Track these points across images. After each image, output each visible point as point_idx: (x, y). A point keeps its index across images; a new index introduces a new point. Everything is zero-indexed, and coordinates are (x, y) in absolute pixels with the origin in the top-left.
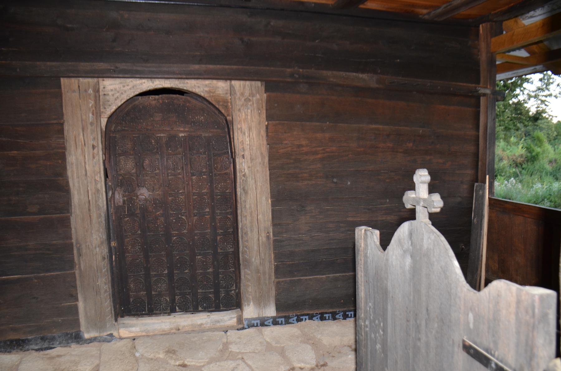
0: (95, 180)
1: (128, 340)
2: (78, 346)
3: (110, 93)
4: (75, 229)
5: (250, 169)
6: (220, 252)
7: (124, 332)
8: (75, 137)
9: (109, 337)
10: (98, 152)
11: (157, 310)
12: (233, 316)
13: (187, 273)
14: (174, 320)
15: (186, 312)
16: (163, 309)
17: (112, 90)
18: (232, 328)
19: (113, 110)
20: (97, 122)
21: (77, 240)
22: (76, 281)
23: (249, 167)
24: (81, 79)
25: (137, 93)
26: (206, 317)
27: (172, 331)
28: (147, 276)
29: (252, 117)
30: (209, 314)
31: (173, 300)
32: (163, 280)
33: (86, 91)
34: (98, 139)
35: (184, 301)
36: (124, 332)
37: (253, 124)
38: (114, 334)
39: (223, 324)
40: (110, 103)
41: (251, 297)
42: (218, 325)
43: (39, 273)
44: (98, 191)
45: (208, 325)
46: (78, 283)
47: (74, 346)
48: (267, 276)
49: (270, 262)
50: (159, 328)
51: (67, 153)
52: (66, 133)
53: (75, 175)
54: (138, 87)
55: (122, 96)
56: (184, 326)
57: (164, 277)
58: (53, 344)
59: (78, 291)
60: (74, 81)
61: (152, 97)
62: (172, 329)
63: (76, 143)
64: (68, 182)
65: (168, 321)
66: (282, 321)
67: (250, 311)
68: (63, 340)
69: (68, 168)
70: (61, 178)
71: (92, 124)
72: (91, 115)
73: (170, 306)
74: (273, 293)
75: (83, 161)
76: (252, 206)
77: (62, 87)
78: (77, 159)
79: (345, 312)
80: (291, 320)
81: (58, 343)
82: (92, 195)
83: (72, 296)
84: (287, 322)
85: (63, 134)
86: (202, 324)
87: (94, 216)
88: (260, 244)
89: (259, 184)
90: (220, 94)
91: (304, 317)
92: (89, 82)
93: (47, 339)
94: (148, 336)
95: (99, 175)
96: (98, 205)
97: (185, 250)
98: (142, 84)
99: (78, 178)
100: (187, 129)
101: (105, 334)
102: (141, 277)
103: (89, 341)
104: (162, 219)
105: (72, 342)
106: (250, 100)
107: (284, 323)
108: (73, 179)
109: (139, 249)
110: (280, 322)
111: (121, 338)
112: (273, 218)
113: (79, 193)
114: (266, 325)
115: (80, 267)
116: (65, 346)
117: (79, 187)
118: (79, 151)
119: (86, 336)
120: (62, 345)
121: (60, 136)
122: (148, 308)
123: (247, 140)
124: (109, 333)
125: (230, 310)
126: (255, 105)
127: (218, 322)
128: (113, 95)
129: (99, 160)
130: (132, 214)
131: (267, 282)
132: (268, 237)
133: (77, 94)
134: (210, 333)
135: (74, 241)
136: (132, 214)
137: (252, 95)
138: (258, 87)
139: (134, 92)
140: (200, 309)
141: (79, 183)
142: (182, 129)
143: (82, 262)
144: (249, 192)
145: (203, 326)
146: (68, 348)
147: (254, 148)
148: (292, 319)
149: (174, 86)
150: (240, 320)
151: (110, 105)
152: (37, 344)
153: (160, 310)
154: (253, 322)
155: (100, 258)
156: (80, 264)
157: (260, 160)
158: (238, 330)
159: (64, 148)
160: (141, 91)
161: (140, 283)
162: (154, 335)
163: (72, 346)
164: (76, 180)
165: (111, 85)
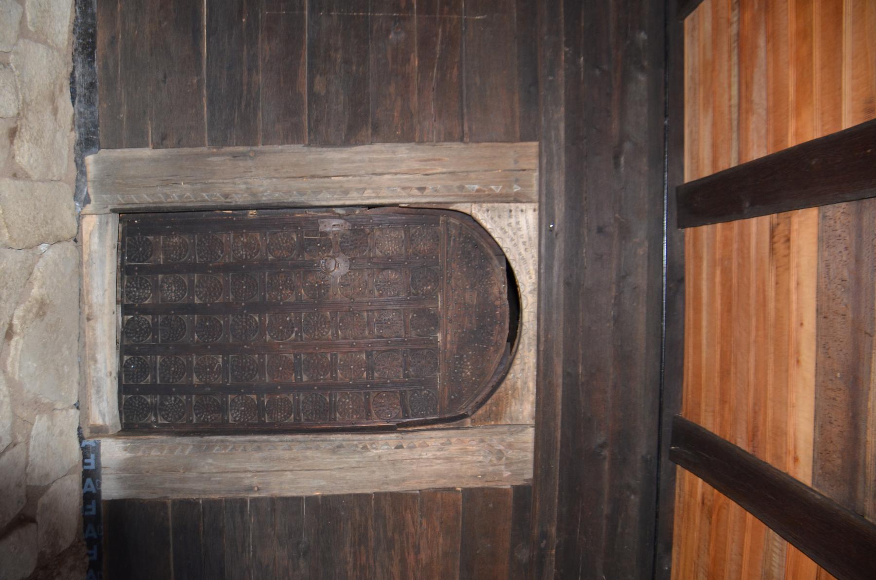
0: (365, 189)
1: (75, 231)
2: (73, 143)
4: (282, 151)
6: (227, 398)
7: (91, 223)
8: (439, 160)
9: (83, 197)
10: (413, 196)
11: (128, 281)
12: (107, 419)
13: (193, 338)
14: (106, 312)
15: (122, 333)
17: (518, 223)
18: (85, 415)
21: (262, 153)
22: (190, 147)
23: (380, 457)
24: (536, 174)
25: (513, 265)
26: (109, 369)
27: (86, 308)
28: (191, 268)
29: (469, 462)
30: (114, 374)
31: (144, 311)
34: (435, 196)
35: (141, 330)
36: (91, 223)
37: (457, 466)
38: (88, 205)
39: (93, 399)
40: (496, 219)
41: (140, 454)
44: (346, 192)
45: (93, 373)
46: (186, 150)
47: (74, 136)
49: (204, 492)
50: (95, 285)
51: (413, 144)
52: (447, 144)
53: (375, 156)
54: (523, 266)
55: (508, 240)
56: (94, 329)
57: (188, 297)
58: (80, 101)
59: (170, 150)
60: (534, 163)
61: (504, 287)
62: (90, 307)
63: (429, 160)
64: (363, 143)
65: (107, 300)
66: (90, 510)
68: (85, 118)
69: (388, 145)
70: (370, 132)
72: (477, 187)
75: (398, 170)
76: (309, 462)
77: (523, 144)
78: (402, 160)
81: (82, 110)
82: (339, 182)
83: (164, 138)
85: (445, 141)
86: (96, 361)
87: (304, 184)
89: (349, 475)
92: (531, 186)
94: (80, 264)
95: (373, 195)
96: (322, 191)
97: (234, 336)
98: (528, 273)
99: (370, 161)
100: (448, 346)
101: (91, 191)
102: (190, 257)
103: (80, 162)
104: (292, 299)
105: (80, 134)
107: (87, 513)
108: (368, 152)
109: (242, 255)
110: (89, 507)
111: (80, 218)
113: (343, 161)
114: (84, 481)
115: (214, 155)
116: (74, 122)
117: (354, 162)
118: (416, 165)
119: (90, 159)
120: (77, 116)
121: (442, 136)
122: (133, 267)
123: (430, 455)
124: (92, 197)
125: (120, 412)
126: (491, 469)
127: (98, 392)
128: (509, 225)
129: (399, 197)
130: (302, 247)
132: (250, 489)
134: (76, 377)
135: (260, 147)
136: (302, 247)
138: (523, 474)
139: (515, 260)
140: (126, 358)
141: (361, 161)
142: (449, 338)
143: (223, 158)
144: (335, 457)
145: (91, 363)
146: (70, 127)
147: (414, 467)
149: (524, 328)
150: (99, 431)
151: (492, 218)
154: (92, 456)
155: (227, 189)
157: (392, 477)
158: (79, 428)
159: (421, 142)
160: (516, 272)
161: (180, 254)
162: (81, 276)
163: (73, 133)
164: (366, 157)
165: (527, 222)
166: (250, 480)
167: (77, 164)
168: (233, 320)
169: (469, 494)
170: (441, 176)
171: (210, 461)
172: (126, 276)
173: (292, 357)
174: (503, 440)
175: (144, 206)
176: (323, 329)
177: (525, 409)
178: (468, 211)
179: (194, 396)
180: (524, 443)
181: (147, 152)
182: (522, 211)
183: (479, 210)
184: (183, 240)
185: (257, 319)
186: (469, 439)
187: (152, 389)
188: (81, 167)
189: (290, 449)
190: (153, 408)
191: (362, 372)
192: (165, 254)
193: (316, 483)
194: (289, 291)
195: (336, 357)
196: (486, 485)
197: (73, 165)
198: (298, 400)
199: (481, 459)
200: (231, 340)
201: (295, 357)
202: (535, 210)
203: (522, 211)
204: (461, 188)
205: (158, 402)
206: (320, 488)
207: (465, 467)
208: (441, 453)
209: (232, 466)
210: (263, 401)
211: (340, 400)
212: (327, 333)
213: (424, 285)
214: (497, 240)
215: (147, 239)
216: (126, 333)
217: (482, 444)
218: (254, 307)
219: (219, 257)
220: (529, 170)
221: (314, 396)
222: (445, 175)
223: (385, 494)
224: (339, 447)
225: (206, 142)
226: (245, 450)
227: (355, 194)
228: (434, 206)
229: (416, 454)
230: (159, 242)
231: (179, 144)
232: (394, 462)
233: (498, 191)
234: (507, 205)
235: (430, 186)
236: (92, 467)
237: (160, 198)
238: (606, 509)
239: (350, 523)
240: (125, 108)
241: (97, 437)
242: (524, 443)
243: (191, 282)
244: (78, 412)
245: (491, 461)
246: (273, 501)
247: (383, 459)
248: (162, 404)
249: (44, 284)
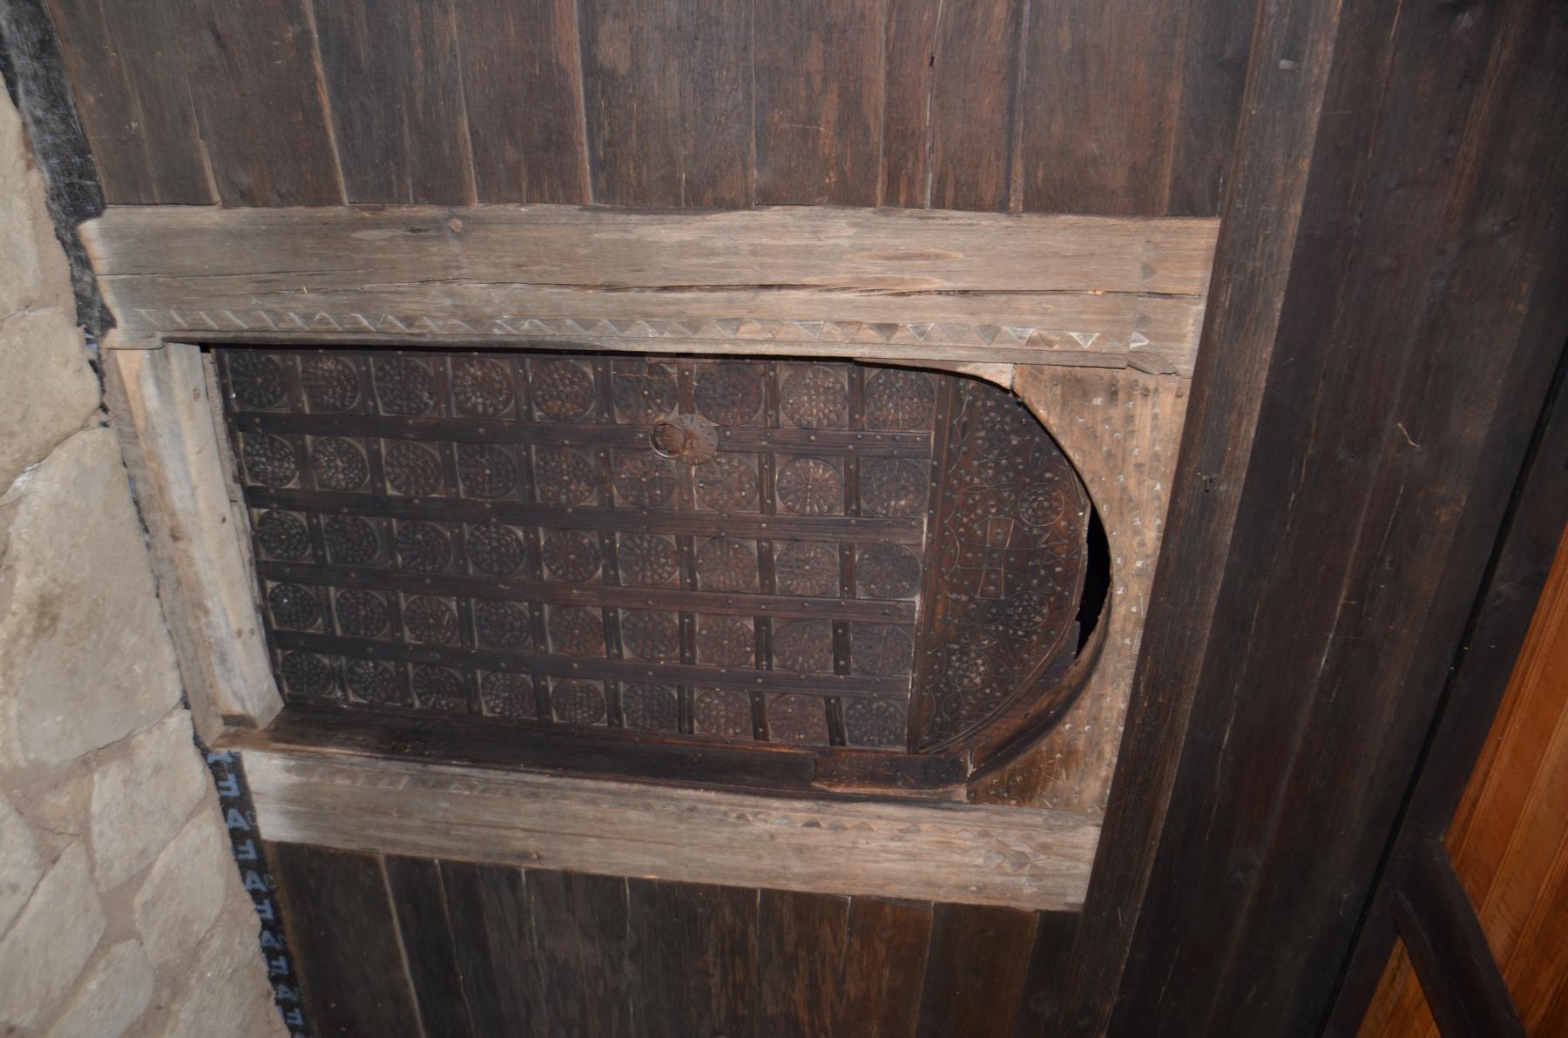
0: (740, 321)
2: (42, 197)
3: (1117, 413)
5: (766, 838)
8: (937, 256)
11: (247, 444)
13: (395, 560)
16: (255, 464)
17: (1129, 419)
19: (1042, 413)
21: (481, 222)
24: (1201, 307)
25: (1104, 511)
26: (234, 627)
28: (370, 426)
29: (953, 864)
32: (362, 479)
33: (1143, 321)
35: (290, 537)
37: (928, 868)
38: (112, 331)
41: (315, 779)
42: (214, 659)
43: (325, 52)
44: (694, 325)
46: (299, 212)
47: (39, 180)
48: (390, 835)
49: (440, 849)
50: (171, 477)
51: (866, 212)
58: (28, 92)
60: (1199, 277)
67: (266, 770)
68: (52, 133)
71: (991, 331)
72: (1031, 332)
73: (265, 490)
74: (337, 843)
75: (826, 279)
77: (1177, 223)
79: (299, 1005)
80: (251, 875)
81: (39, 113)
84: (244, 867)
86: (207, 612)
87: (589, 301)
88: (501, 832)
90: (1057, 777)
91: (267, 906)
92: (1180, 338)
93: (47, 68)
96: (633, 321)
97: (477, 564)
99: (754, 253)
103: (68, 238)
104: (592, 502)
105: (51, 171)
106: (1021, 866)
112: (593, 878)
116: (28, 144)
118: (874, 269)
119: (89, 229)
120: (33, 129)
124: (117, 313)
125: (276, 677)
126: (998, 879)
130: (606, 394)
131: (371, 832)
132: (524, 855)
133: (1136, 282)
136: (606, 394)
137: (1038, 875)
138: (1064, 895)
143: (388, 233)
146: (21, 164)
147: (841, 860)
148: (256, 878)
150: (239, 725)
151: (1064, 405)
152: (17, 22)
153: (247, 454)
155: (411, 306)
156: (377, 225)
157: (796, 870)
158: (196, 737)
160: (1107, 528)
161: (343, 396)
166: (519, 842)
167: (64, 244)
168: (472, 535)
169: (953, 914)
171: (445, 805)
172: (240, 434)
173: (598, 612)
174: (1030, 838)
175: (231, 335)
176: (662, 566)
177: (1093, 784)
179: (410, 666)
180: (1075, 847)
181: (209, 217)
184: (346, 366)
185: (520, 534)
186: (956, 828)
187: (329, 644)
188: (74, 248)
189: (594, 802)
190: (337, 677)
191: (748, 654)
192: (309, 394)
193: (647, 861)
194: (583, 486)
195: (692, 623)
196: (985, 902)
197: (56, 250)
198: (616, 693)
199: (980, 861)
200: (471, 571)
201: (605, 614)
205: (345, 668)
206: (654, 869)
207: (944, 870)
208: (899, 844)
209: (488, 817)
210: (546, 688)
211: (700, 700)
212: (671, 574)
213: (890, 498)
215: (269, 361)
216: (263, 541)
217: (984, 840)
218: (509, 514)
219: (427, 405)
220: (1181, 296)
221: (647, 687)
222: (950, 299)
223: (782, 893)
224: (692, 809)
225: (345, 198)
226: (507, 794)
227: (718, 332)
229: (845, 840)
230: (294, 367)
231: (286, 200)
232: (800, 850)
233: (1087, 345)
235: (906, 320)
236: (234, 793)
237: (259, 319)
239: (713, 924)
240: (137, 107)
241: (234, 744)
242: (1075, 847)
243: (375, 455)
244: (187, 714)
245: (1000, 866)
246: (568, 877)
247: (780, 840)
248: (351, 671)
249: (38, 563)
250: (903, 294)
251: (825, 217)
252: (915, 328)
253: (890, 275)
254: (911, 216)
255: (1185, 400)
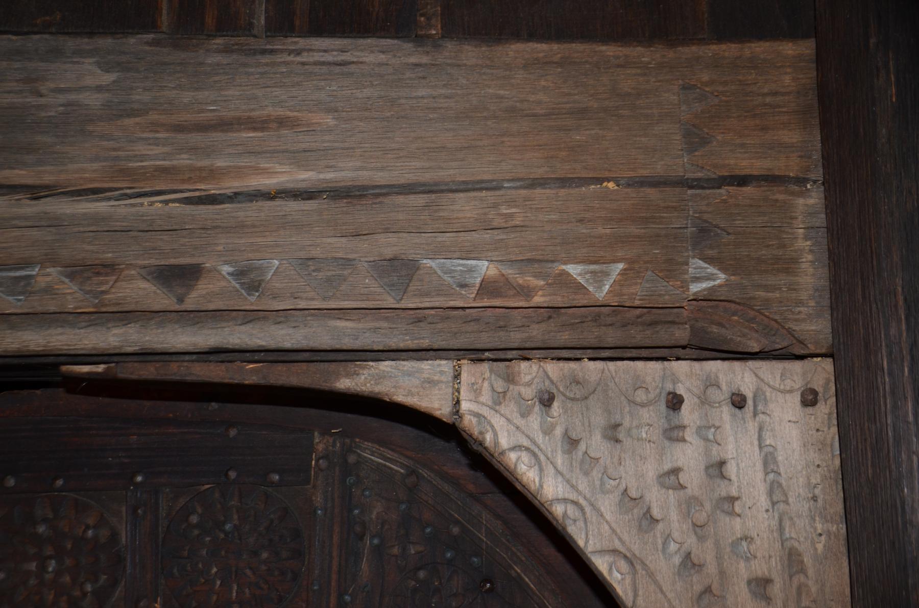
3: (689, 456)
17: (718, 469)
20: (418, 317)
24: (812, 201)
33: (704, 237)
40: (596, 444)
72: (485, 268)
77: (729, 50)
128: (671, 477)
133: (677, 163)
151: (572, 443)
165: (769, 462)
170: (293, 206)
178: (436, 403)
182: (738, 402)
183: (499, 398)
202: (810, 399)
203: (738, 402)
204: (399, 270)
214: (601, 564)
228: (250, 374)
233: (602, 292)
234: (651, 371)
238: (340, 165)
250: (212, 200)
251: (56, 54)
252: (239, 274)
253: (184, 160)
254: (227, 50)
255: (826, 408)
